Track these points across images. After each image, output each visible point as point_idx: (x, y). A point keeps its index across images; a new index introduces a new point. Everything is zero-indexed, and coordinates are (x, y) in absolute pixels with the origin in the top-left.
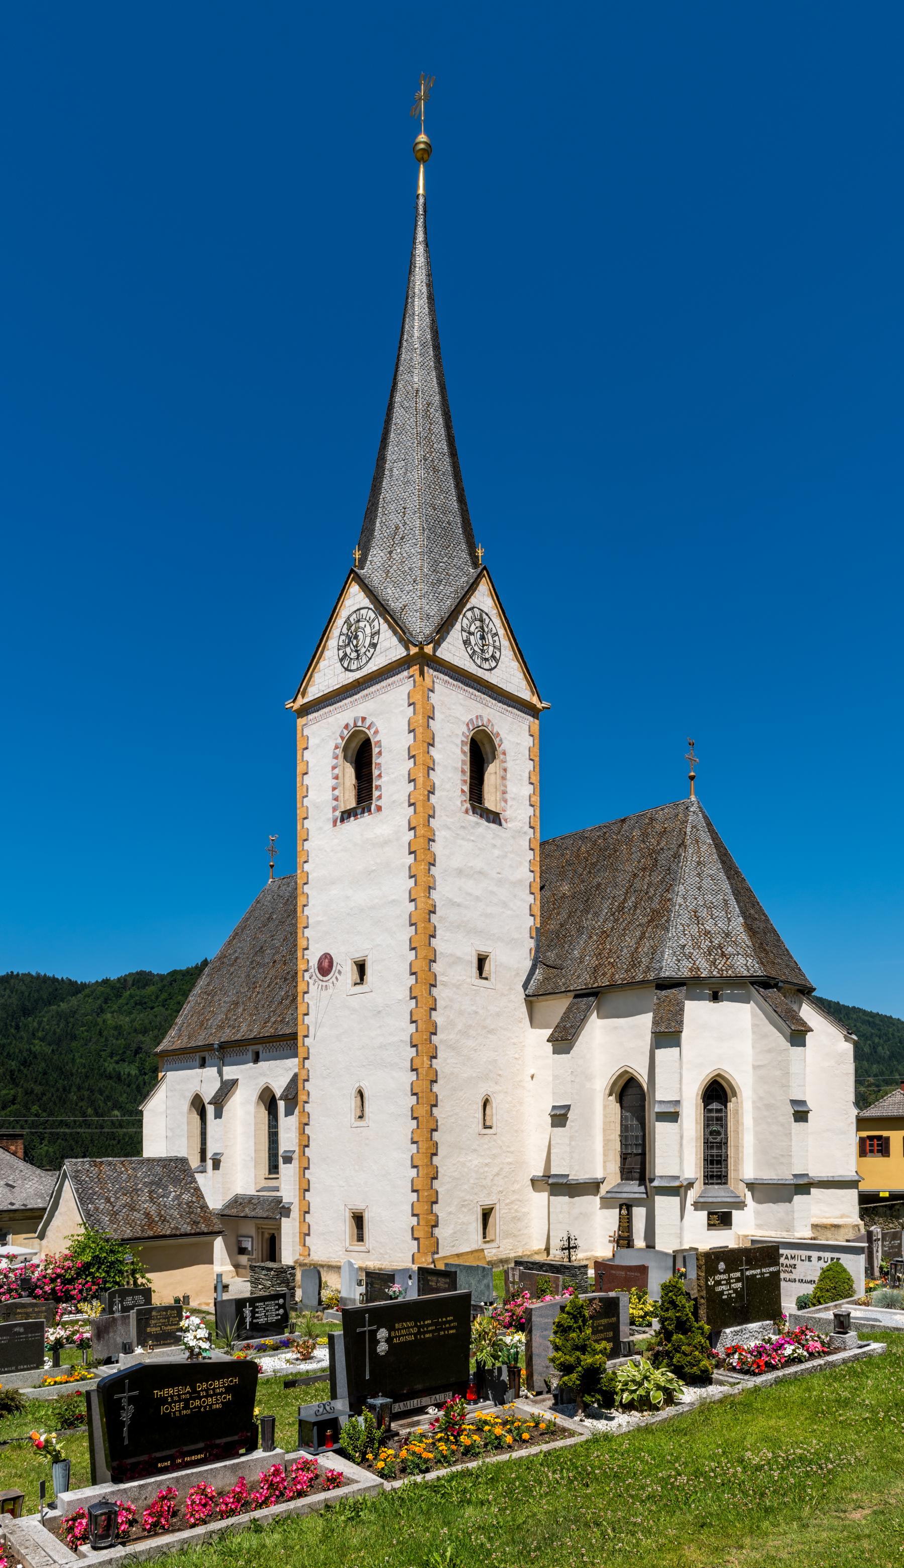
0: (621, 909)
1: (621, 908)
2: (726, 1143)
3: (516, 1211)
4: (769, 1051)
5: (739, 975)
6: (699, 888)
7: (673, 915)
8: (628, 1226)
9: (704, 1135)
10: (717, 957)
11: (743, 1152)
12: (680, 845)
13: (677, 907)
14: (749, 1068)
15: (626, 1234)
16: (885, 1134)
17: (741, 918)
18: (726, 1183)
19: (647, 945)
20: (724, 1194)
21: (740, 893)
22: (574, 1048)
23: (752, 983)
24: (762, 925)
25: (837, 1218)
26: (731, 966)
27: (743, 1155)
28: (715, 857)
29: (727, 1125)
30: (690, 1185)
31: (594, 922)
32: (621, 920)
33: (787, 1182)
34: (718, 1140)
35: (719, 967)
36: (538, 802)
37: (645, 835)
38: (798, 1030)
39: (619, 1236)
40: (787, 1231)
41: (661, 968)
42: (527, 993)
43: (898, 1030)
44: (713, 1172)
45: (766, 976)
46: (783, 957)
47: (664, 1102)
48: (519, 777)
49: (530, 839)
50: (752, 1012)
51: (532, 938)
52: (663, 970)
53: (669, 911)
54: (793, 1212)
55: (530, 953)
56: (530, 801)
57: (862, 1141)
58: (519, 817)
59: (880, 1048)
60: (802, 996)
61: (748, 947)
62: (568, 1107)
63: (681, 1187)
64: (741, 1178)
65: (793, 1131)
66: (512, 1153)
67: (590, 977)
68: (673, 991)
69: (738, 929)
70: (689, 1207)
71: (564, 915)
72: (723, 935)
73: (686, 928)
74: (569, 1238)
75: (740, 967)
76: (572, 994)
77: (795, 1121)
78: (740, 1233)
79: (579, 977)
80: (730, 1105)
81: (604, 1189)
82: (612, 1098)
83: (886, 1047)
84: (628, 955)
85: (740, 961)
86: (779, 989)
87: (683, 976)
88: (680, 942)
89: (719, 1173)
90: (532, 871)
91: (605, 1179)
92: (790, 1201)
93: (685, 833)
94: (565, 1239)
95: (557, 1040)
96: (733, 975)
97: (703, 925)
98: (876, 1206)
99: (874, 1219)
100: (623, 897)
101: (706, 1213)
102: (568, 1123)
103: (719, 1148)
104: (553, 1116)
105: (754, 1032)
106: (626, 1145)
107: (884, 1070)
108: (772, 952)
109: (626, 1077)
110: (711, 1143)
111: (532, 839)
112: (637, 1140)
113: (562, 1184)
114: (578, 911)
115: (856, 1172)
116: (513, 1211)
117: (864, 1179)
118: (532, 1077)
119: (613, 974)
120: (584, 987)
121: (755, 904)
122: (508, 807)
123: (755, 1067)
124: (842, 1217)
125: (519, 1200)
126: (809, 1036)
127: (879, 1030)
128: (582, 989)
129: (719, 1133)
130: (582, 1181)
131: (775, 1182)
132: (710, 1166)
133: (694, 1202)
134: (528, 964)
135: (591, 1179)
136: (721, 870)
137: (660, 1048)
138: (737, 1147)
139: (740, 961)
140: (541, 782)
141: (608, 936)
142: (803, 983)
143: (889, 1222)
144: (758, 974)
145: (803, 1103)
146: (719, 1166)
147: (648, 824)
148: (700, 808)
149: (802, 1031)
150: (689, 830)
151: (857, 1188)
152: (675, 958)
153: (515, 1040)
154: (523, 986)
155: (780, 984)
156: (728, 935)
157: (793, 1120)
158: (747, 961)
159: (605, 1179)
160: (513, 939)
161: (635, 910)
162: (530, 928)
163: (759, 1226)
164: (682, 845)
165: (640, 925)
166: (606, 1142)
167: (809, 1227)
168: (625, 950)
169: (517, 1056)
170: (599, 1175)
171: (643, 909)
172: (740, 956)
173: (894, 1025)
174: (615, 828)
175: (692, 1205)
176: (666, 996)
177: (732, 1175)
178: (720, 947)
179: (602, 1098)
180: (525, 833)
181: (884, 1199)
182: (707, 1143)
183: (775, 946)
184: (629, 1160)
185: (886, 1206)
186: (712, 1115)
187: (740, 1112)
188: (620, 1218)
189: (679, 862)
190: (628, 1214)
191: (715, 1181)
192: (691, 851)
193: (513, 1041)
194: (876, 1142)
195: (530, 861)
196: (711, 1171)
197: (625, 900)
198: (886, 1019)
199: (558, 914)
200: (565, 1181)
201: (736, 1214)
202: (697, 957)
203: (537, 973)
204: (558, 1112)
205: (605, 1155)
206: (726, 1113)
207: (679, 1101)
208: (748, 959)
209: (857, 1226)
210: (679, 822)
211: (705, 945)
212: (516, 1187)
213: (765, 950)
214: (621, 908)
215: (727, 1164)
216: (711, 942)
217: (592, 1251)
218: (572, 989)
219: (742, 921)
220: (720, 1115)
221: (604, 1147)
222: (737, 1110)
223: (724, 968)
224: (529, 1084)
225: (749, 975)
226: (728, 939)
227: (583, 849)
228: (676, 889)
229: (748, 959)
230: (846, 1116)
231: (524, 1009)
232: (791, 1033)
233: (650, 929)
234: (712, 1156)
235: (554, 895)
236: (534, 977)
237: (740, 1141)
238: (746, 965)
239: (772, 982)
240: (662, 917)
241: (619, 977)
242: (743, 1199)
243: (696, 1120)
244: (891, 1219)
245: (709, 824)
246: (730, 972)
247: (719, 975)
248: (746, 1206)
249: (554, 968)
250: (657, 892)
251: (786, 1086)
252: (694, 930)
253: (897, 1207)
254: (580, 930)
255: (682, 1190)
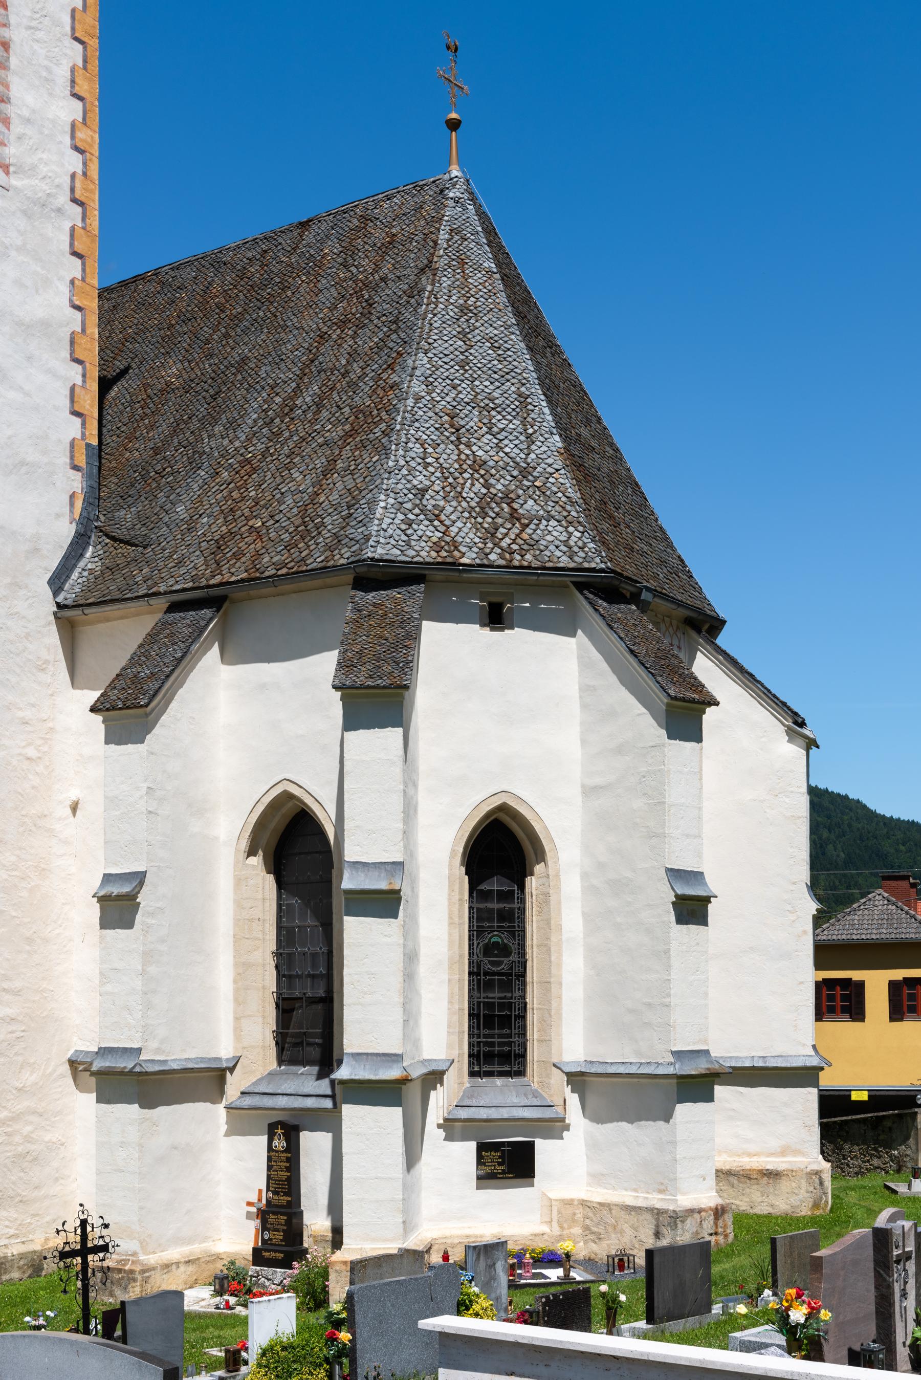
0: (287, 410)
1: (288, 409)
2: (523, 975)
3: (28, 1139)
4: (619, 750)
5: (550, 565)
6: (463, 365)
7: (399, 419)
8: (289, 1179)
9: (471, 954)
10: (500, 521)
11: (560, 997)
12: (422, 270)
13: (410, 402)
14: (575, 793)
15: (284, 1199)
16: (855, 975)
17: (557, 438)
18: (521, 1073)
19: (339, 485)
20: (516, 1101)
21: (558, 387)
22: (157, 730)
23: (581, 587)
24: (607, 466)
25: (772, 1154)
26: (533, 544)
27: (560, 1004)
28: (502, 298)
29: (523, 931)
30: (434, 1078)
31: (226, 442)
32: (286, 434)
33: (661, 1071)
34: (504, 967)
35: (504, 544)
36: (96, 147)
37: (349, 251)
38: (683, 700)
39: (268, 1202)
40: (661, 1191)
41: (367, 538)
42: (60, 599)
43: (857, 819)
44: (492, 1044)
45: (613, 571)
46: (654, 542)
47: (364, 864)
48: (44, 74)
49: (73, 230)
50: (580, 657)
51: (75, 468)
52: (371, 543)
53: (391, 410)
54: (674, 1143)
55: (72, 505)
56: (73, 137)
57: (821, 987)
58: (43, 169)
59: (830, 847)
60: (694, 634)
61: (573, 503)
62: (139, 878)
63: (404, 1081)
64: (555, 1060)
65: (674, 946)
66: (17, 993)
67: (206, 564)
68: (393, 593)
69: (550, 461)
70: (433, 1133)
71: (164, 427)
72: (515, 473)
73: (430, 450)
74: (84, 1223)
75: (552, 548)
76: (162, 603)
77: (677, 923)
78: (552, 1195)
79: (180, 563)
80: (533, 884)
81: (234, 1085)
82: (256, 861)
83: (839, 846)
84: (295, 510)
85: (553, 533)
86: (644, 607)
87: (416, 559)
88: (415, 482)
89: (506, 1049)
90: (78, 308)
91: (237, 1060)
92: (667, 1117)
93: (436, 243)
94: (70, 1227)
95: (114, 708)
96: (536, 564)
97: (469, 446)
98: (846, 1121)
99: (841, 1149)
100: (294, 385)
101: (472, 1146)
102: (139, 918)
103: (507, 986)
104: (104, 900)
105: (584, 706)
106: (290, 977)
107: (837, 883)
108: (628, 527)
109: (288, 810)
110: (486, 974)
111: (79, 232)
112: (314, 965)
113: (122, 1073)
114: (194, 419)
115: (814, 1047)
116: (17, 1139)
117: (830, 1065)
118: (74, 808)
119: (258, 554)
120: (190, 585)
121: (592, 418)
122: (12, 138)
123: (589, 791)
124: (783, 1152)
125: (34, 1113)
126: (710, 716)
127: (829, 817)
128: (184, 590)
129: (505, 951)
130: (175, 1066)
131: (633, 1070)
132: (483, 1032)
133: (446, 1120)
134: (66, 531)
135: (202, 1060)
136: (516, 330)
137: (355, 729)
138: (546, 984)
139: (553, 533)
140: (102, 97)
141: (254, 470)
142: (698, 603)
143: (872, 1155)
144: (593, 565)
145: (696, 877)
146: (506, 1031)
147: (358, 229)
148: (471, 193)
149: (693, 701)
150: (443, 236)
151: (814, 1083)
152: (400, 516)
153: (27, 714)
154: (51, 582)
155: (645, 595)
156: (525, 472)
157: (673, 918)
158: (570, 534)
159: (237, 1060)
160: (23, 463)
161: (318, 412)
162: (72, 444)
163: (597, 1178)
164: (428, 268)
165: (326, 443)
166: (242, 968)
167: (712, 1180)
168: (289, 501)
169: (31, 752)
170: (224, 1051)
171: (334, 409)
172: (553, 523)
173: (851, 810)
174: (286, 241)
175: (439, 1126)
176: (375, 605)
177: (534, 1052)
178: (508, 498)
179: (231, 860)
180: (59, 210)
181: (860, 1106)
182: (478, 974)
183: (637, 515)
184: (297, 1014)
185: (865, 1120)
186: (490, 905)
187: (553, 899)
188: (269, 1159)
189: (419, 305)
190: (287, 1150)
191: (496, 1068)
192: (446, 282)
193: (20, 714)
194: (839, 991)
195: (72, 282)
196: (486, 1044)
197: (298, 391)
198: (839, 800)
199: (152, 427)
200: (130, 1065)
201: (544, 1149)
202: (453, 517)
203: (88, 554)
204: (116, 889)
205: (238, 1001)
206: (523, 901)
207: (401, 864)
208: (571, 529)
209: (817, 1173)
210: (423, 222)
211: (473, 490)
212: (29, 1078)
213: (611, 517)
214: (288, 409)
215: (524, 1027)
216: (487, 485)
217: (205, 1239)
218: (162, 590)
219: (560, 445)
220: (508, 906)
221: (235, 982)
222: (547, 895)
223: (515, 547)
224: (69, 827)
225: (572, 565)
226: (526, 483)
227: (216, 288)
228: (410, 362)
229: (571, 529)
230: (792, 917)
231: (52, 638)
232: (668, 705)
233: (347, 452)
234: (489, 1006)
235: (146, 386)
236: (81, 564)
237: (554, 971)
238: (566, 543)
239: (627, 589)
240: (376, 424)
241: (270, 561)
242: (560, 1110)
243: (450, 918)
244: (875, 1149)
245: (490, 232)
246: (528, 557)
247: (502, 562)
248: (567, 1128)
249: (128, 543)
250: (368, 370)
251: (656, 836)
252: (449, 455)
253: (888, 1123)
254: (194, 465)
255: (413, 1092)
